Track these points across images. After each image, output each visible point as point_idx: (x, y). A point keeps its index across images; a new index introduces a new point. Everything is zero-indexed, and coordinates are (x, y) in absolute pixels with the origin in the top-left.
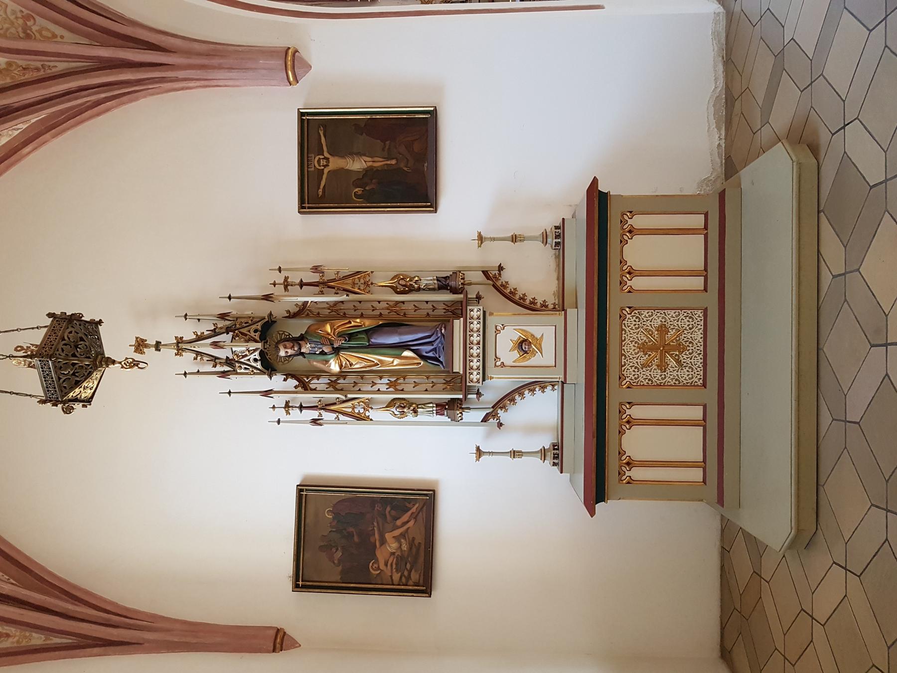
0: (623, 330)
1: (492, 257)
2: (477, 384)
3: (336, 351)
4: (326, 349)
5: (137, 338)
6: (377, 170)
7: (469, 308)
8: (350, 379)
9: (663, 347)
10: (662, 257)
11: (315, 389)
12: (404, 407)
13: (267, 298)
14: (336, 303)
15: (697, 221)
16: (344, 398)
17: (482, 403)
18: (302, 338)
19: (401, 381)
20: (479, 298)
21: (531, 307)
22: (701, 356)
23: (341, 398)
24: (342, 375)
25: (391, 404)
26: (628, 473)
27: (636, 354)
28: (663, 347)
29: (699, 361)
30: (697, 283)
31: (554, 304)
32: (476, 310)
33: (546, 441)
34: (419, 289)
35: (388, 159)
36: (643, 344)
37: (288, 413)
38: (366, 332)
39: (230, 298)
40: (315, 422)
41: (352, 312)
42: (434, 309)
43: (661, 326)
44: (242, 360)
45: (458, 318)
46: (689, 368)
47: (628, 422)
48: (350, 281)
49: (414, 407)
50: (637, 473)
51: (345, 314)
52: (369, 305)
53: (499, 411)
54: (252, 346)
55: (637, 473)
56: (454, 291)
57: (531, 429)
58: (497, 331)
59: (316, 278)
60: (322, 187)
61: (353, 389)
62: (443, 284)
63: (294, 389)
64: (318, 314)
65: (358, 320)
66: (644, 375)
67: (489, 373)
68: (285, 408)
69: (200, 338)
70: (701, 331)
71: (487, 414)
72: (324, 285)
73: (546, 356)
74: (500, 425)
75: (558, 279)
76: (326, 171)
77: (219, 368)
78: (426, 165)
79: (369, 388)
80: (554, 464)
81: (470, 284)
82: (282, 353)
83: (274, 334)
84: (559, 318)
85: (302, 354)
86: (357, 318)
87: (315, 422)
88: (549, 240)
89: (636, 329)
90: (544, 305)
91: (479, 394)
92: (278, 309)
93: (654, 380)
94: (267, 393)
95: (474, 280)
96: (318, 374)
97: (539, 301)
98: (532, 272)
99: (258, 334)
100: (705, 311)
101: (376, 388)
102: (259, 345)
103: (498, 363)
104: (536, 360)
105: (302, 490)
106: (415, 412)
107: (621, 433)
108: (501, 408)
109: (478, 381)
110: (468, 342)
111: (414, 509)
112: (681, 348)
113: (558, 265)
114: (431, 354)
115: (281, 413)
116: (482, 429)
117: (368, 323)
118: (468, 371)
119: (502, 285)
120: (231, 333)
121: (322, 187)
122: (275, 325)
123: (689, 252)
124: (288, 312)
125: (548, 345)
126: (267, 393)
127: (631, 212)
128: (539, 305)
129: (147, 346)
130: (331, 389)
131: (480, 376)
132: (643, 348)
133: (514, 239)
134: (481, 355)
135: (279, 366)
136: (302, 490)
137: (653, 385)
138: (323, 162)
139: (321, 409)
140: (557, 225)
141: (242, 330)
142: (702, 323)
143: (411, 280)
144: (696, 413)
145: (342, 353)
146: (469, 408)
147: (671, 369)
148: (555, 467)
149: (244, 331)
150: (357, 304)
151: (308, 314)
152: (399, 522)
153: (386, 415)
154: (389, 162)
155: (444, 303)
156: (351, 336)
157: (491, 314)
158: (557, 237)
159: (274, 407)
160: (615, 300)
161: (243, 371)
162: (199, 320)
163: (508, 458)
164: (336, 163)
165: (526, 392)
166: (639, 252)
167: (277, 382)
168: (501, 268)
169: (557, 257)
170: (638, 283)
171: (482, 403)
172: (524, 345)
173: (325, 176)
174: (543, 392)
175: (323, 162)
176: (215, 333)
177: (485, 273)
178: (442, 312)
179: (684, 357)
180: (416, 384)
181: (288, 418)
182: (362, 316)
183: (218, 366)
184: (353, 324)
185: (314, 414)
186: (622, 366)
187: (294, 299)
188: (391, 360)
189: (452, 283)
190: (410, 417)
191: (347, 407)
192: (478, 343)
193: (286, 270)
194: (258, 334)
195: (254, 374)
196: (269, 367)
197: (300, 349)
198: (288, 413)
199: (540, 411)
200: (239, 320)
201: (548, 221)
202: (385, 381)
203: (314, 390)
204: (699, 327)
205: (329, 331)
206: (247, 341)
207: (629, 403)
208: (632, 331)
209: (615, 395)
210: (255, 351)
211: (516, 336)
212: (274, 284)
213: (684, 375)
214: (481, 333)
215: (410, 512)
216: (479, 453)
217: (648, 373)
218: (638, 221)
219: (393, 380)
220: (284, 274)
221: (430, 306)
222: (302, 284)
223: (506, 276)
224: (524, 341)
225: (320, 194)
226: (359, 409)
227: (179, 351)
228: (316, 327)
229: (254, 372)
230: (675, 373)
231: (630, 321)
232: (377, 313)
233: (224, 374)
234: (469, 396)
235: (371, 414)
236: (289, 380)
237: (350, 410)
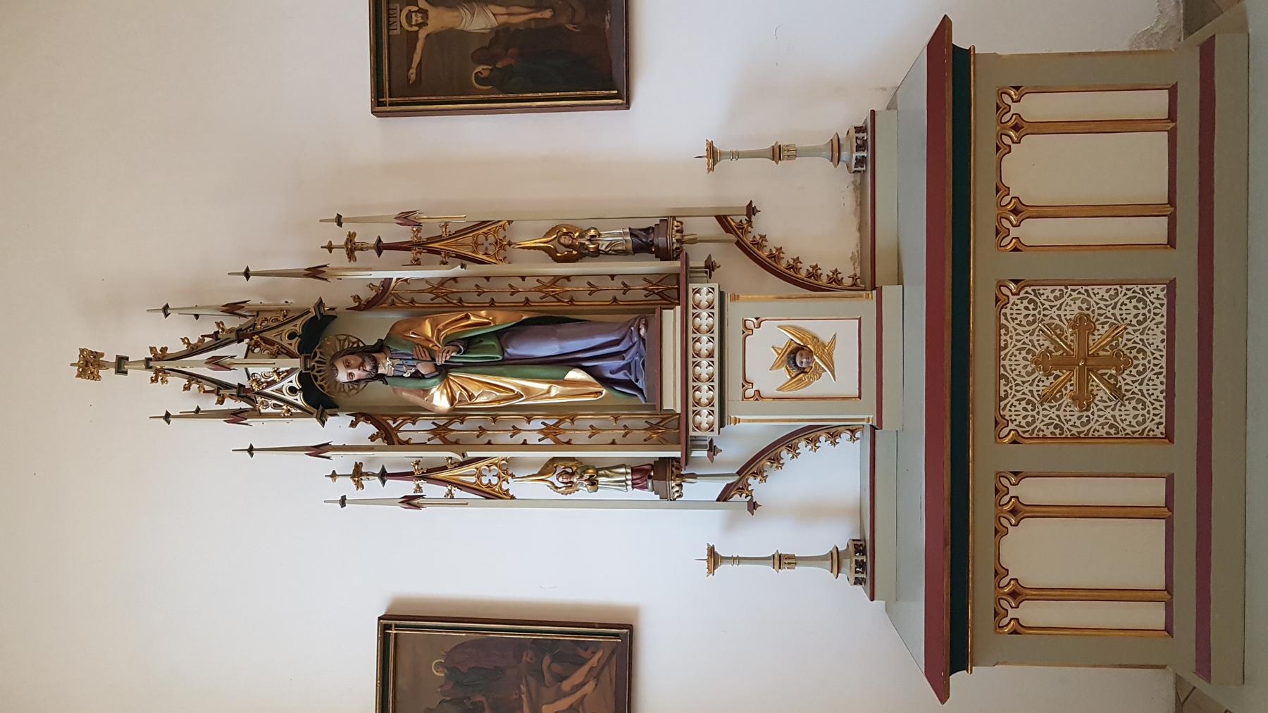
0: (1001, 326)
1: (734, 188)
2: (709, 434)
3: (443, 372)
4: (424, 369)
5: (82, 351)
6: (518, 31)
7: (692, 286)
8: (473, 422)
9: (1083, 361)
10: (1080, 177)
11: (407, 442)
12: (573, 474)
13: (315, 273)
14: (443, 281)
16: (460, 459)
17: (721, 464)
18: (381, 347)
19: (566, 424)
20: (710, 267)
21: (811, 283)
23: (455, 460)
24: (457, 414)
25: (548, 468)
26: (1012, 613)
27: (1028, 374)
28: (1083, 361)
29: (1158, 386)
30: (1155, 229)
31: (854, 277)
32: (705, 290)
33: (839, 536)
34: (597, 253)
35: (539, 7)
36: (1043, 354)
37: (359, 485)
38: (498, 334)
39: (247, 274)
40: (409, 501)
41: (474, 298)
42: (626, 288)
43: (1080, 318)
44: (268, 391)
45: (671, 306)
46: (1139, 403)
47: (1013, 512)
48: (468, 239)
49: (591, 474)
50: (1031, 613)
51: (460, 301)
52: (504, 284)
53: (751, 480)
54: (285, 364)
55: (1031, 613)
56: (664, 254)
57: (812, 512)
58: (747, 331)
59: (404, 234)
60: (415, 64)
61: (479, 441)
62: (644, 242)
63: (369, 443)
64: (412, 301)
65: (483, 313)
66: (1044, 418)
67: (731, 412)
68: (353, 476)
69: (193, 350)
70: (1162, 327)
71: (728, 486)
72: (421, 248)
73: (841, 378)
74: (753, 506)
75: (860, 229)
76: (422, 34)
77: (231, 404)
78: (608, 17)
79: (504, 438)
80: (858, 582)
81: (694, 241)
82: (342, 376)
83: (330, 343)
84: (867, 304)
85: (382, 377)
86: (483, 308)
87: (409, 501)
88: (845, 155)
89: (1029, 323)
90: (835, 279)
91: (712, 449)
92: (336, 295)
94: (318, 451)
95: (700, 234)
96: (413, 413)
97: (826, 271)
98: (810, 216)
99: (295, 341)
101: (519, 438)
102: (296, 363)
103: (750, 393)
104: (822, 385)
105: (387, 627)
106: (593, 483)
107: (999, 532)
108: (755, 475)
109: (711, 428)
110: (691, 352)
111: (594, 661)
112: (1121, 361)
113: (861, 204)
114: (620, 376)
115: (346, 486)
116: (718, 515)
117: (502, 319)
118: (691, 408)
119: (754, 243)
120: (247, 340)
121: (415, 64)
122: (336, 322)
123: (1140, 167)
124: (356, 298)
125: (846, 356)
126: (318, 451)
127: (1017, 88)
128: (824, 279)
129: (101, 365)
130: (437, 441)
131: (715, 419)
132: (1044, 362)
133: (777, 154)
134: (716, 377)
135: (341, 398)
136: (387, 627)
137: (1060, 437)
138: (417, 18)
139: (420, 478)
141: (266, 335)
142: (1164, 310)
143: (581, 236)
144: (1153, 492)
145: (453, 375)
146: (694, 476)
147: (1101, 405)
148: (859, 587)
149: (269, 335)
150: (482, 283)
151: (393, 304)
152: (566, 686)
153: (540, 489)
154: (538, 15)
155: (645, 277)
156: (470, 344)
157: (735, 298)
159: (334, 475)
160: (987, 266)
161: (270, 410)
162: (197, 316)
163: (767, 569)
164: (440, 19)
165: (802, 444)
166: (1032, 169)
167: (338, 428)
168: (751, 210)
169: (859, 188)
171: (721, 464)
172: (799, 358)
173: (420, 45)
174: (834, 443)
175: (417, 18)
176: (218, 340)
177: (722, 220)
178: (641, 295)
179: (1126, 381)
180: (594, 430)
181: (360, 494)
182: (492, 305)
183: (227, 401)
184: (473, 319)
185: (408, 488)
186: (1001, 399)
187: (364, 275)
188: (545, 386)
189: (660, 241)
190: (584, 492)
191: (467, 474)
192: (710, 355)
193: (349, 220)
194: (295, 341)
195: (292, 415)
196: (320, 401)
197: (376, 367)
198: (359, 485)
199: (829, 476)
200: (262, 316)
201: (840, 118)
202: (537, 424)
203: (406, 444)
204: (1158, 319)
205: (430, 334)
206: (275, 355)
207: (1015, 474)
208: (1020, 329)
209: (986, 457)
210: (289, 373)
211: (784, 339)
212: (330, 248)
213: (1127, 416)
214: (716, 335)
215: (586, 668)
216: (714, 559)
217: (1053, 413)
218: (1032, 107)
219: (551, 422)
221: (617, 283)
222: (380, 247)
223: (761, 225)
224: (800, 348)
225: (413, 77)
226: (490, 478)
227: (160, 375)
228: (405, 326)
229: (292, 411)
230: (1108, 413)
231: (1017, 308)
232: (520, 298)
233: (236, 417)
234: (695, 454)
235: (512, 486)
236: (362, 424)
237: (473, 480)
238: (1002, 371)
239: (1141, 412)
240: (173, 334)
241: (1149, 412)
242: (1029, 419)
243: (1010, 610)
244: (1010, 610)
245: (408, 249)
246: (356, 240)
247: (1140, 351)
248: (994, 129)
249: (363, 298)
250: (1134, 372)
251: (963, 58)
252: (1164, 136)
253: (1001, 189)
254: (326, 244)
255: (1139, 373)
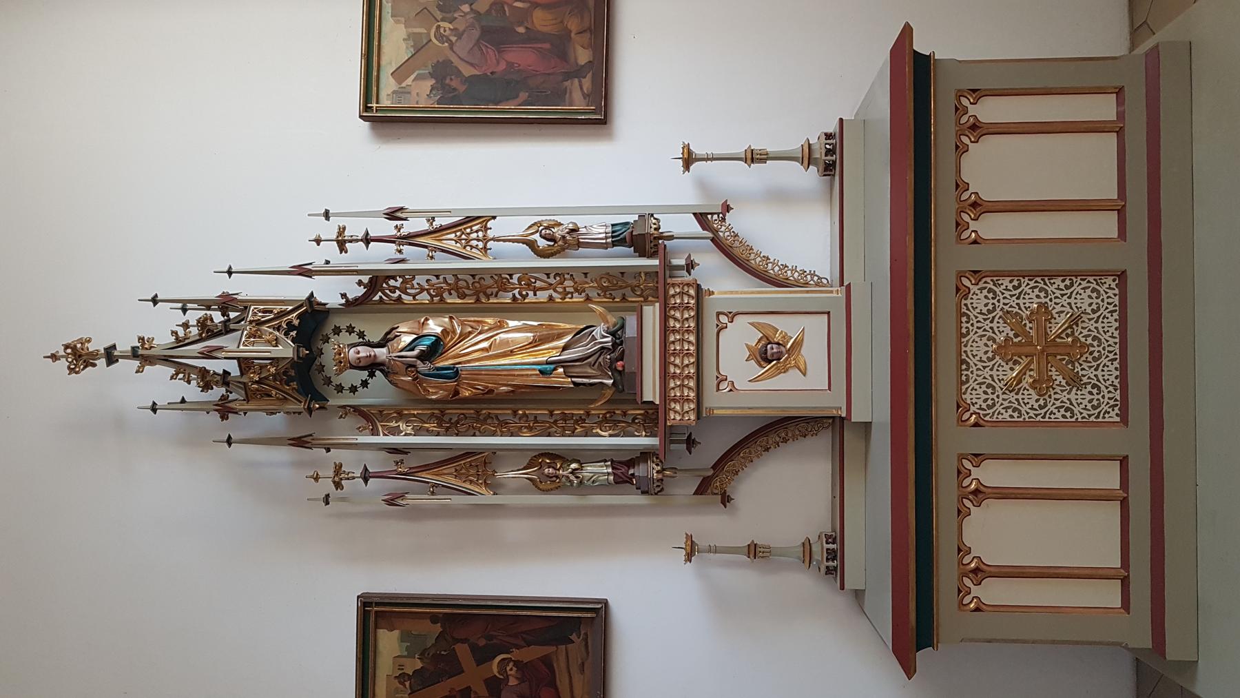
10: (1036, 176)
15: (1103, 108)
22: (1116, 364)
29: (1111, 373)
46: (1091, 396)
92: (329, 292)
93: (1024, 409)
100: (1121, 276)
103: (724, 319)
123: (1089, 167)
125: (814, 353)
140: (830, 130)
142: (1116, 300)
158: (828, 159)
160: (948, 260)
166: (990, 168)
170: (992, 592)
177: (701, 217)
186: (963, 383)
209: (950, 440)
211: (754, 337)
218: (988, 111)
220: (335, 222)
231: (978, 300)
238: (964, 357)
239: (1096, 397)
240: (162, 327)
241: (1103, 397)
242: (990, 402)
243: (971, 222)
244: (971, 222)
245: (393, 242)
246: (346, 233)
247: (1095, 338)
248: (952, 130)
249: (350, 296)
250: (1090, 359)
251: (923, 64)
252: (1112, 139)
253: (961, 186)
254: (313, 237)
255: (1095, 359)
